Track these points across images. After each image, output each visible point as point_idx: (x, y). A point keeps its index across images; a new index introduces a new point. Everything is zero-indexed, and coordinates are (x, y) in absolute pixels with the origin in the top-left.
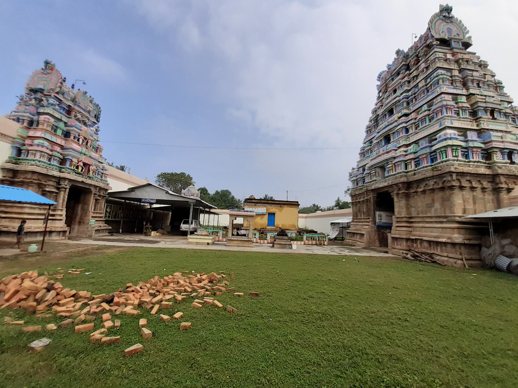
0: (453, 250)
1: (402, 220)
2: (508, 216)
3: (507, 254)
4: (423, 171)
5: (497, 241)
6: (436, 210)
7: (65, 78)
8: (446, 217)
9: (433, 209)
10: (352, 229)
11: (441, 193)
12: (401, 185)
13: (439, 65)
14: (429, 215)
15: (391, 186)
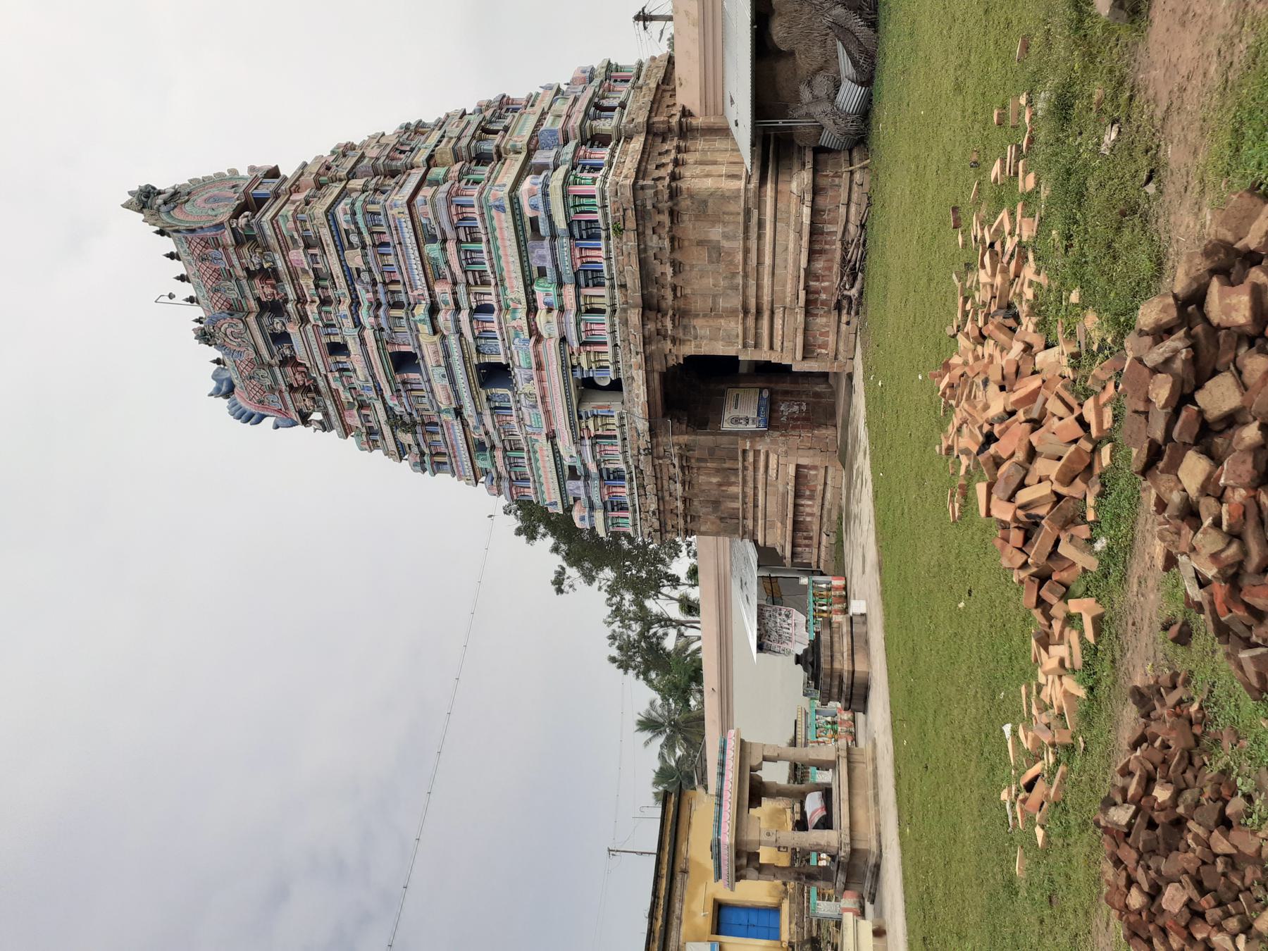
0: (830, 193)
1: (752, 332)
2: (749, 69)
3: (832, 90)
4: (617, 261)
5: (803, 111)
6: (726, 236)
7: (214, 362)
8: (747, 212)
9: (726, 244)
10: (779, 538)
11: (686, 218)
12: (651, 326)
13: (319, 209)
14: (740, 257)
15: (648, 359)
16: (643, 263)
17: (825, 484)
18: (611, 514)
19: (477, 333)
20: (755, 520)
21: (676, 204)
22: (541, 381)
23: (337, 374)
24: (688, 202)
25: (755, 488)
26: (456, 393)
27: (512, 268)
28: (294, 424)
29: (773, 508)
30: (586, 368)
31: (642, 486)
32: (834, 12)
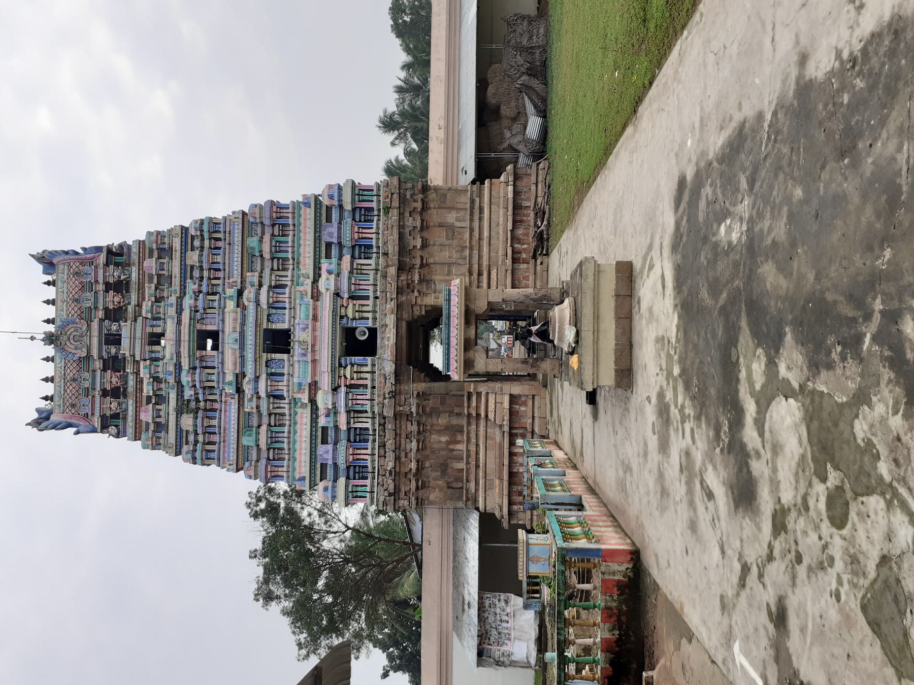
4: (383, 235)
6: (458, 220)
8: (472, 201)
10: (495, 500)
12: (403, 277)
14: (467, 235)
15: (399, 306)
16: (401, 237)
17: (533, 418)
18: (353, 482)
19: (271, 301)
20: (477, 484)
21: (425, 197)
22: (314, 330)
23: (148, 362)
24: (434, 195)
25: (477, 445)
26: (242, 357)
27: (308, 255)
28: (94, 431)
29: (492, 465)
30: (348, 376)
31: (383, 445)
32: (522, 78)
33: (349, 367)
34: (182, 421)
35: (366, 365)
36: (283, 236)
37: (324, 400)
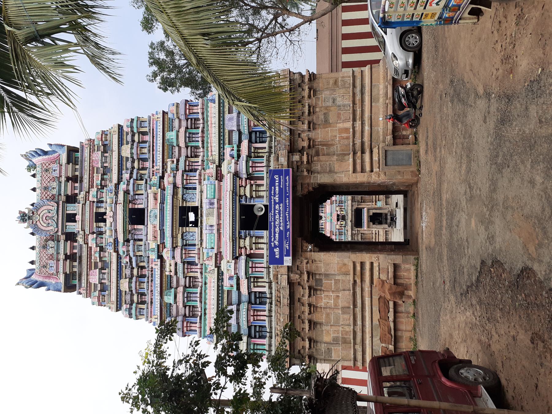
33: (248, 239)
34: (121, 285)
35: (265, 311)
36: (195, 128)
37: (227, 266)
